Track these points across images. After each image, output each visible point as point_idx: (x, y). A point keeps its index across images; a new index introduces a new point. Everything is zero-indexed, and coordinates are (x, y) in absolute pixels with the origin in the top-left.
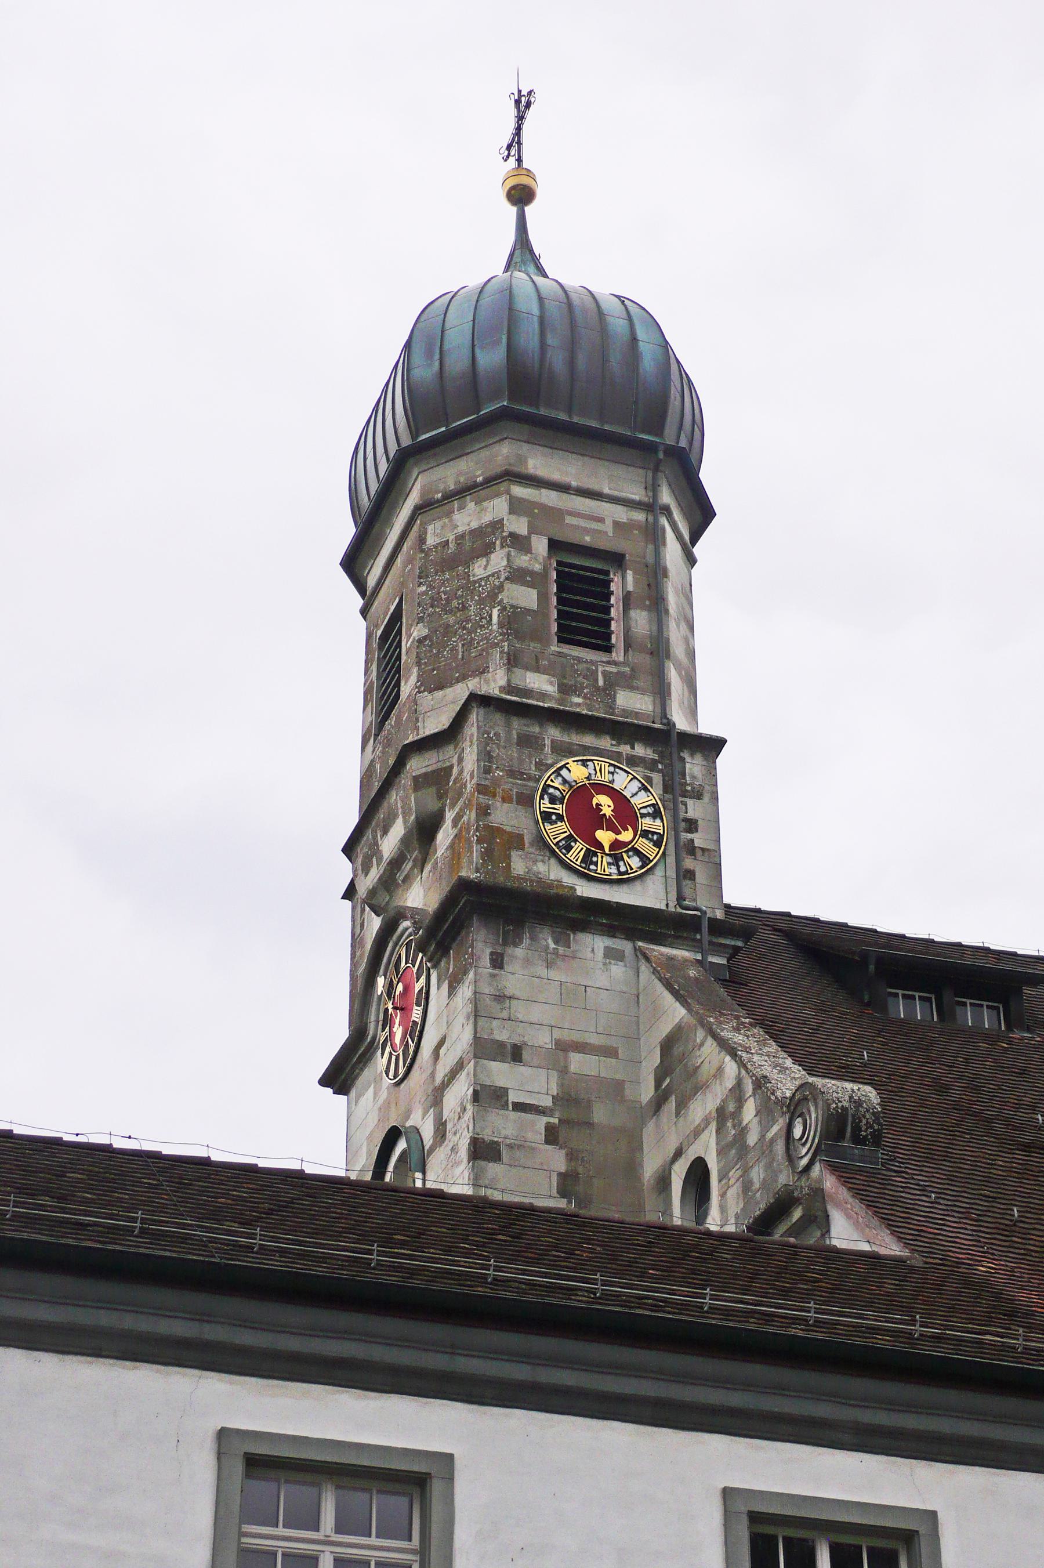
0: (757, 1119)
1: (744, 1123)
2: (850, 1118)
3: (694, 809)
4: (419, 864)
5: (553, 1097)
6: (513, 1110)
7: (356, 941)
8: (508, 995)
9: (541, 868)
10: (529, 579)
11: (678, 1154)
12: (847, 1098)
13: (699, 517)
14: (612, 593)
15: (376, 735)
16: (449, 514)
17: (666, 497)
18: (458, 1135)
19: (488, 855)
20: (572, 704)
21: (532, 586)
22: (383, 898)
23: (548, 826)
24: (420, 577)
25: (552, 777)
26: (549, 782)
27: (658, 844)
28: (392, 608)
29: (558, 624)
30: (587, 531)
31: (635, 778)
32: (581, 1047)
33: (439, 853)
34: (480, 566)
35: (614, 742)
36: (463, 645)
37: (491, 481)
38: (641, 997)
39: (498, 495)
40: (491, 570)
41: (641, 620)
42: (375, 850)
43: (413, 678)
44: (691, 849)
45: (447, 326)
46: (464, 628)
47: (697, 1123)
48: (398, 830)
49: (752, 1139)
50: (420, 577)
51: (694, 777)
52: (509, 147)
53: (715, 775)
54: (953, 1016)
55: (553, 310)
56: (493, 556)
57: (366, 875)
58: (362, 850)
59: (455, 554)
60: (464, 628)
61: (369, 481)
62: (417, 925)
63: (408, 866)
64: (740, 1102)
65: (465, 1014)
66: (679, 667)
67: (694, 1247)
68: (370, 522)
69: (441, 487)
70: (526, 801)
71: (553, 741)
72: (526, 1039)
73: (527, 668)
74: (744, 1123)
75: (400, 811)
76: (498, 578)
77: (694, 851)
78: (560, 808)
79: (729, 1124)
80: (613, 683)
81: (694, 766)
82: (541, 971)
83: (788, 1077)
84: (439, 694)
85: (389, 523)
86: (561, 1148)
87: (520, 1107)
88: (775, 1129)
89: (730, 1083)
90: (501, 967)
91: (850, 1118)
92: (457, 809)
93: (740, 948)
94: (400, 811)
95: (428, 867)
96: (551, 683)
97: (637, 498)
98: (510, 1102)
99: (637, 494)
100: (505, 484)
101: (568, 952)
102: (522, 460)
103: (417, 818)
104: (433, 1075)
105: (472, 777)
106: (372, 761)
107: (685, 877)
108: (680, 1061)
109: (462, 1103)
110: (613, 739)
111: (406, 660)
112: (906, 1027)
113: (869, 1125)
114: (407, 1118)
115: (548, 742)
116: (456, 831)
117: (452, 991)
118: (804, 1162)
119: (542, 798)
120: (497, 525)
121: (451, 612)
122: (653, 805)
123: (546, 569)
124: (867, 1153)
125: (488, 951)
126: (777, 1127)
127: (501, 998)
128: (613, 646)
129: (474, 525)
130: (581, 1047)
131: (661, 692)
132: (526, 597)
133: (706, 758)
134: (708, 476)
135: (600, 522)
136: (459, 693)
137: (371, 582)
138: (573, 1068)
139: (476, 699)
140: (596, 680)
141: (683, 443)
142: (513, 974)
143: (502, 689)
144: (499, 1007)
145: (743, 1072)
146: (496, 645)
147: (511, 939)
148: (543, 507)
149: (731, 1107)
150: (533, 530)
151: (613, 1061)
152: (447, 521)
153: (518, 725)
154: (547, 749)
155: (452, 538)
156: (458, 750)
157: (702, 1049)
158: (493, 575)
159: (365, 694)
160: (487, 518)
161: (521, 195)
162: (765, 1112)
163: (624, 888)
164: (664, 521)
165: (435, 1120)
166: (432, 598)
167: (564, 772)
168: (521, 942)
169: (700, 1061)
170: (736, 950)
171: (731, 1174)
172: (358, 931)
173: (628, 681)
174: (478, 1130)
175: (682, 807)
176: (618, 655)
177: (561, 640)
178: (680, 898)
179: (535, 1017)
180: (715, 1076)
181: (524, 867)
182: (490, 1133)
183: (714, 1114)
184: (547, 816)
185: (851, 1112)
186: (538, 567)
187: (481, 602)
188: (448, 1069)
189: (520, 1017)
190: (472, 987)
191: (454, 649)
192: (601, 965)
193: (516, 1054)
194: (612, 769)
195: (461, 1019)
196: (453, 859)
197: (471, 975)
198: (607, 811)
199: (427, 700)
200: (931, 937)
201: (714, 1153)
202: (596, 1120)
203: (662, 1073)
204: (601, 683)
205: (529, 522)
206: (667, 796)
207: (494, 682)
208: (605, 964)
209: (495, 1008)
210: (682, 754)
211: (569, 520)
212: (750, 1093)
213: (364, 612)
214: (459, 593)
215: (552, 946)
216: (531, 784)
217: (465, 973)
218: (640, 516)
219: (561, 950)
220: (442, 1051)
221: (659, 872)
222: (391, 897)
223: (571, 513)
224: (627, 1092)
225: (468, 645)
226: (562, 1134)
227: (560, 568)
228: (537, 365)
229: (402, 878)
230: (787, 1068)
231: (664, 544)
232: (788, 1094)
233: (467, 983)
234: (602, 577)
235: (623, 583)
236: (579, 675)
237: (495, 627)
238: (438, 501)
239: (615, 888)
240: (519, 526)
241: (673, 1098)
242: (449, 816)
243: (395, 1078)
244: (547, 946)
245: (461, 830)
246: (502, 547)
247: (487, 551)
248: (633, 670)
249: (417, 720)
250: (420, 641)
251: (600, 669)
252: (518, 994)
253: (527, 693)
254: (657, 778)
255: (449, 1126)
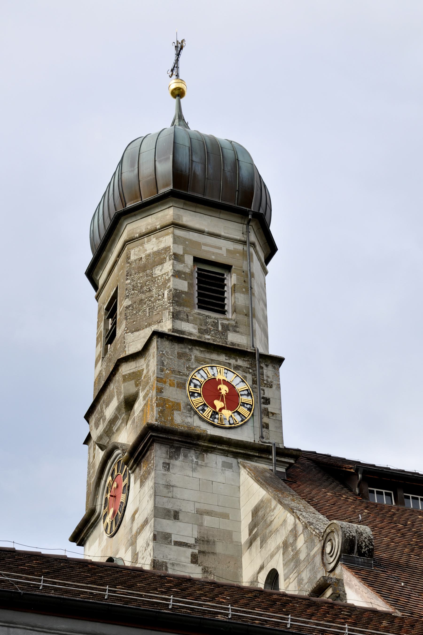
0: (305, 545)
1: (298, 548)
2: (357, 542)
3: (268, 393)
4: (125, 421)
5: (195, 539)
6: (175, 545)
7: (90, 465)
8: (172, 484)
9: (189, 420)
10: (183, 276)
11: (262, 568)
12: (355, 531)
13: (269, 251)
14: (225, 285)
15: (103, 358)
16: (142, 244)
17: (253, 238)
18: (145, 559)
19: (161, 413)
20: (205, 338)
21: (185, 280)
22: (104, 442)
23: (193, 399)
24: (127, 276)
25: (195, 374)
26: (193, 377)
27: (250, 410)
28: (112, 294)
29: (198, 299)
30: (213, 254)
31: (238, 376)
32: (209, 513)
33: (136, 415)
34: (158, 270)
35: (227, 358)
36: (149, 309)
37: (164, 227)
38: (241, 487)
39: (168, 234)
40: (163, 272)
41: (241, 299)
42: (102, 416)
43: (123, 326)
44: (267, 413)
45: (141, 151)
46: (150, 300)
47: (272, 550)
48: (114, 403)
49: (302, 556)
50: (127, 276)
51: (268, 377)
52: (172, 70)
53: (279, 376)
54: (403, 504)
55: (196, 144)
56: (165, 264)
57: (97, 429)
58: (93, 419)
59: (145, 264)
60: (150, 300)
61: (105, 207)
62: (124, 451)
63: (119, 422)
64: (296, 537)
65: (149, 495)
66: (259, 323)
67: (279, 600)
68: (101, 252)
69: (139, 231)
70: (181, 386)
71: (195, 357)
72: (181, 508)
73: (182, 320)
74: (298, 548)
75: (115, 394)
76: (168, 275)
77: (267, 411)
78: (199, 390)
79: (290, 549)
80: (226, 328)
81: (268, 371)
82: (190, 473)
83: (321, 522)
84: (137, 333)
85: (110, 250)
86: (199, 566)
87: (178, 544)
88: (316, 549)
89: (290, 527)
90: (168, 470)
91: (357, 542)
92: (145, 391)
93: (292, 464)
94: (115, 394)
95: (130, 423)
96: (194, 328)
97: (238, 238)
98: (172, 541)
99: (239, 236)
100: (172, 228)
101: (203, 463)
102: (179, 217)
103: (125, 396)
104: (131, 529)
105: (154, 374)
106: (101, 371)
107: (263, 427)
108: (263, 518)
109: (147, 542)
110: (226, 356)
111: (119, 318)
112: (380, 507)
113: (366, 546)
114: (117, 553)
115: (193, 357)
116: (145, 402)
117: (142, 484)
118: (332, 565)
119: (190, 384)
120: (167, 249)
121: (143, 293)
122: (247, 390)
123: (192, 272)
124: (366, 561)
125: (162, 461)
126: (318, 547)
127: (168, 486)
128: (226, 311)
129: (155, 249)
130: (209, 513)
131: (253, 334)
132: (183, 285)
133: (274, 368)
134: (275, 229)
135: (218, 250)
136: (147, 333)
137: (101, 282)
138: (205, 524)
139: (156, 334)
140: (218, 327)
141: (261, 211)
142: (174, 474)
143: (169, 330)
144: (167, 491)
145: (297, 521)
146: (167, 309)
147: (174, 455)
148: (190, 241)
149: (291, 540)
150: (186, 252)
151: (227, 520)
152: (141, 247)
153: (177, 348)
154: (193, 360)
155: (143, 256)
156: (147, 361)
157: (275, 511)
158: (165, 274)
159: (97, 339)
160: (162, 246)
161: (178, 93)
162: (310, 541)
163: (232, 431)
164: (252, 250)
165: (132, 553)
166: (133, 286)
167: (201, 372)
168: (179, 455)
169: (273, 518)
170: (291, 464)
171: (291, 576)
172: (91, 460)
173: (235, 329)
174: (156, 555)
175: (262, 392)
176: (229, 315)
177: (199, 307)
178: (262, 437)
179: (186, 497)
180: (281, 525)
181: (180, 420)
182: (162, 557)
183: (281, 545)
184: (192, 394)
185: (357, 538)
186: (188, 270)
187: (159, 287)
188: (139, 525)
189: (178, 496)
190: (153, 481)
191: (144, 311)
192: (220, 470)
193: (176, 516)
194: (226, 371)
195: (147, 498)
196: (143, 417)
197: (153, 474)
198: (223, 392)
199: (130, 337)
200: (388, 467)
201: (282, 566)
202: (217, 552)
203: (253, 526)
204: (220, 328)
205: (183, 248)
206: (255, 385)
207: (166, 326)
208: (222, 470)
209: (165, 491)
210: (262, 365)
211: (203, 248)
212: (301, 532)
213: (97, 298)
214: (147, 283)
215: (195, 460)
216: (185, 377)
217: (149, 473)
218: (240, 247)
219: (200, 462)
220: (136, 516)
221: (250, 424)
222: (110, 439)
223: (205, 245)
224: (234, 537)
225: (152, 309)
226: (201, 558)
227: (200, 272)
228: (187, 171)
229: (116, 429)
230: (320, 519)
231: (253, 262)
232: (322, 531)
233: (150, 479)
234: (220, 277)
235: (231, 280)
236: (209, 325)
237: (166, 300)
238: (137, 238)
239: (228, 431)
240: (180, 250)
241: (259, 539)
242: (141, 395)
243: (110, 533)
244: (192, 460)
245: (147, 401)
246: (170, 260)
247: (162, 262)
248: (236, 323)
249: (125, 347)
250: (127, 308)
251: (220, 322)
252: (177, 484)
253: (182, 332)
254: (249, 376)
255: (140, 555)
